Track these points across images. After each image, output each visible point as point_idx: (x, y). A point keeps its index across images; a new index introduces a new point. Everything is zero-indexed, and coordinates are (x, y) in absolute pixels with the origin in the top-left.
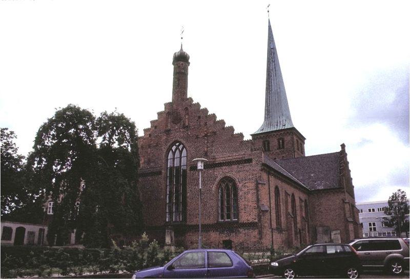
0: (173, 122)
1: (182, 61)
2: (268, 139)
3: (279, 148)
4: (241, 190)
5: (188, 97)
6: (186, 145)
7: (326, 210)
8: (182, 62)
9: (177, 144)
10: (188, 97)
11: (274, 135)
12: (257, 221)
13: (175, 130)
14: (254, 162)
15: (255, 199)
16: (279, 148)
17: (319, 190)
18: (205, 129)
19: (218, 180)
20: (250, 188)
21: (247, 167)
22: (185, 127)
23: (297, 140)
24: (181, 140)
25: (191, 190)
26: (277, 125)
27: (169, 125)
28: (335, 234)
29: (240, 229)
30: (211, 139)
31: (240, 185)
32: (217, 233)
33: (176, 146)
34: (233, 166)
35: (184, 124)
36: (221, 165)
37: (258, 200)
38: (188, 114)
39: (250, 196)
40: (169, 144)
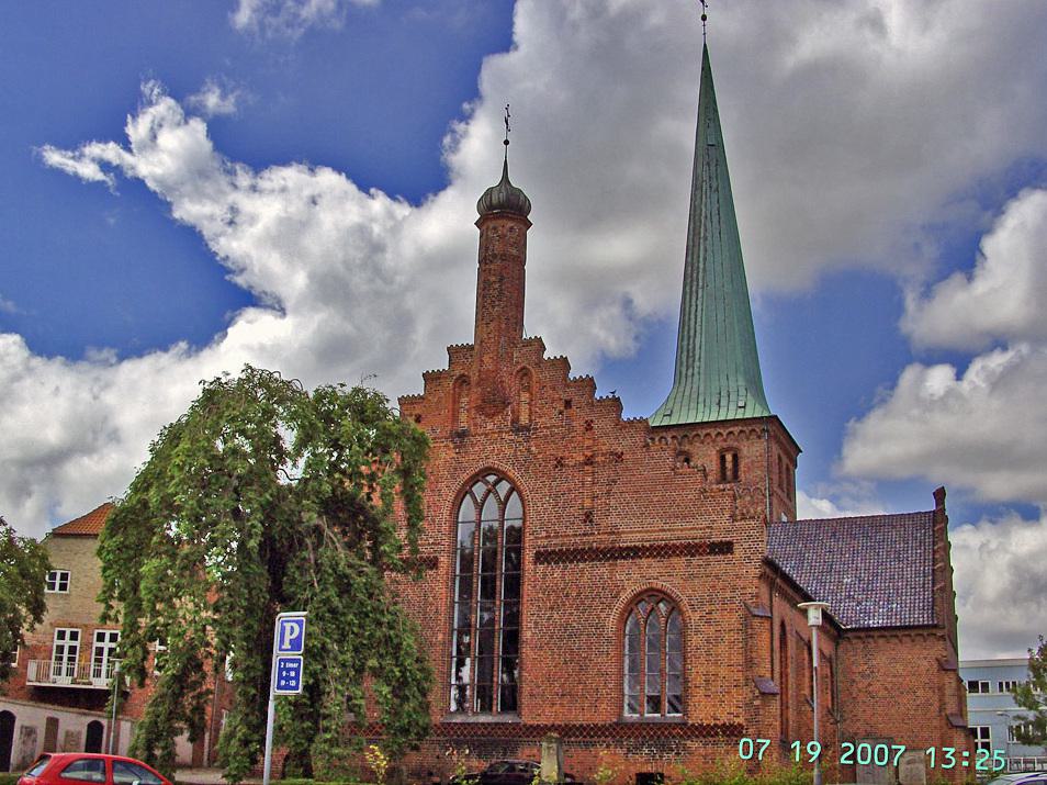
0: (480, 409)
1: (512, 219)
2: (687, 447)
3: (723, 478)
4: (697, 632)
5: (528, 334)
6: (522, 483)
7: (886, 689)
8: (510, 224)
9: (491, 479)
10: (528, 334)
11: (708, 434)
12: (741, 720)
13: (486, 435)
14: (738, 551)
15: (738, 659)
16: (723, 478)
17: (869, 629)
18: (587, 443)
19: (625, 596)
20: (725, 626)
21: (717, 563)
22: (517, 428)
23: (780, 458)
24: (506, 468)
25: (536, 623)
26: (719, 404)
27: (463, 416)
28: (909, 763)
29: (689, 742)
30: (604, 475)
31: (694, 617)
32: (619, 751)
33: (487, 483)
34: (675, 560)
35: (515, 421)
36: (635, 552)
37: (749, 663)
38: (528, 389)
39: (722, 648)
40: (465, 477)
